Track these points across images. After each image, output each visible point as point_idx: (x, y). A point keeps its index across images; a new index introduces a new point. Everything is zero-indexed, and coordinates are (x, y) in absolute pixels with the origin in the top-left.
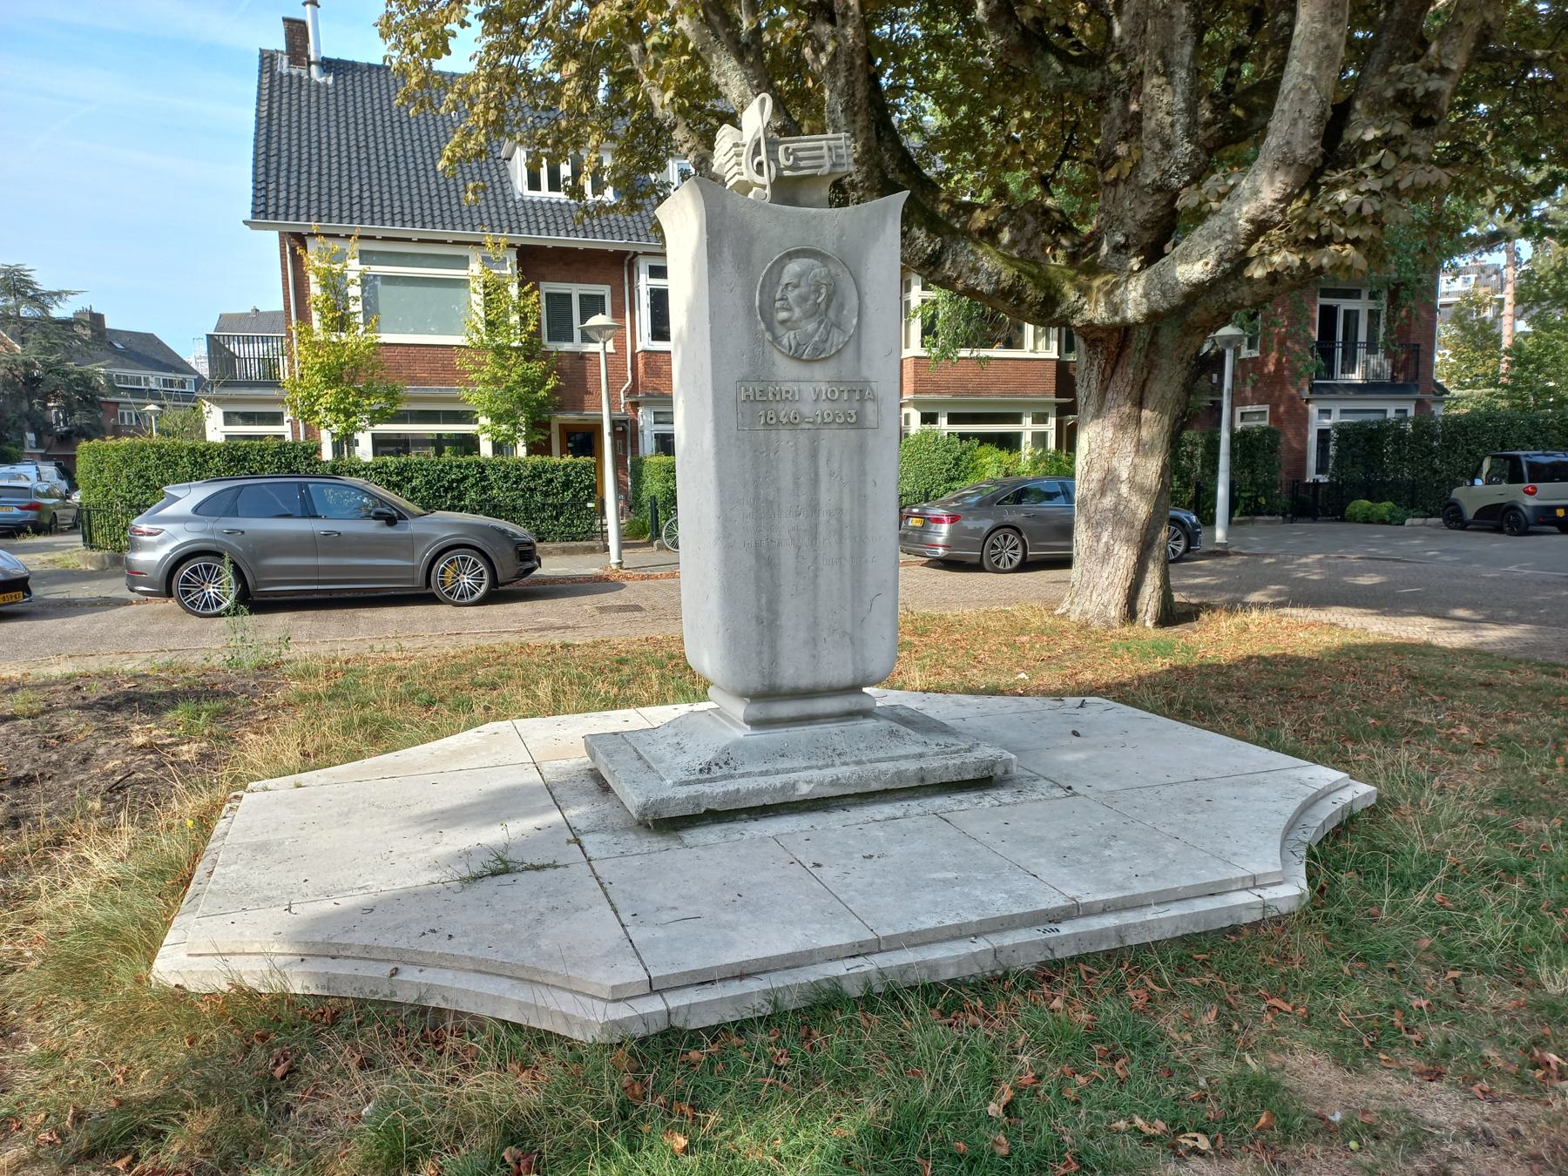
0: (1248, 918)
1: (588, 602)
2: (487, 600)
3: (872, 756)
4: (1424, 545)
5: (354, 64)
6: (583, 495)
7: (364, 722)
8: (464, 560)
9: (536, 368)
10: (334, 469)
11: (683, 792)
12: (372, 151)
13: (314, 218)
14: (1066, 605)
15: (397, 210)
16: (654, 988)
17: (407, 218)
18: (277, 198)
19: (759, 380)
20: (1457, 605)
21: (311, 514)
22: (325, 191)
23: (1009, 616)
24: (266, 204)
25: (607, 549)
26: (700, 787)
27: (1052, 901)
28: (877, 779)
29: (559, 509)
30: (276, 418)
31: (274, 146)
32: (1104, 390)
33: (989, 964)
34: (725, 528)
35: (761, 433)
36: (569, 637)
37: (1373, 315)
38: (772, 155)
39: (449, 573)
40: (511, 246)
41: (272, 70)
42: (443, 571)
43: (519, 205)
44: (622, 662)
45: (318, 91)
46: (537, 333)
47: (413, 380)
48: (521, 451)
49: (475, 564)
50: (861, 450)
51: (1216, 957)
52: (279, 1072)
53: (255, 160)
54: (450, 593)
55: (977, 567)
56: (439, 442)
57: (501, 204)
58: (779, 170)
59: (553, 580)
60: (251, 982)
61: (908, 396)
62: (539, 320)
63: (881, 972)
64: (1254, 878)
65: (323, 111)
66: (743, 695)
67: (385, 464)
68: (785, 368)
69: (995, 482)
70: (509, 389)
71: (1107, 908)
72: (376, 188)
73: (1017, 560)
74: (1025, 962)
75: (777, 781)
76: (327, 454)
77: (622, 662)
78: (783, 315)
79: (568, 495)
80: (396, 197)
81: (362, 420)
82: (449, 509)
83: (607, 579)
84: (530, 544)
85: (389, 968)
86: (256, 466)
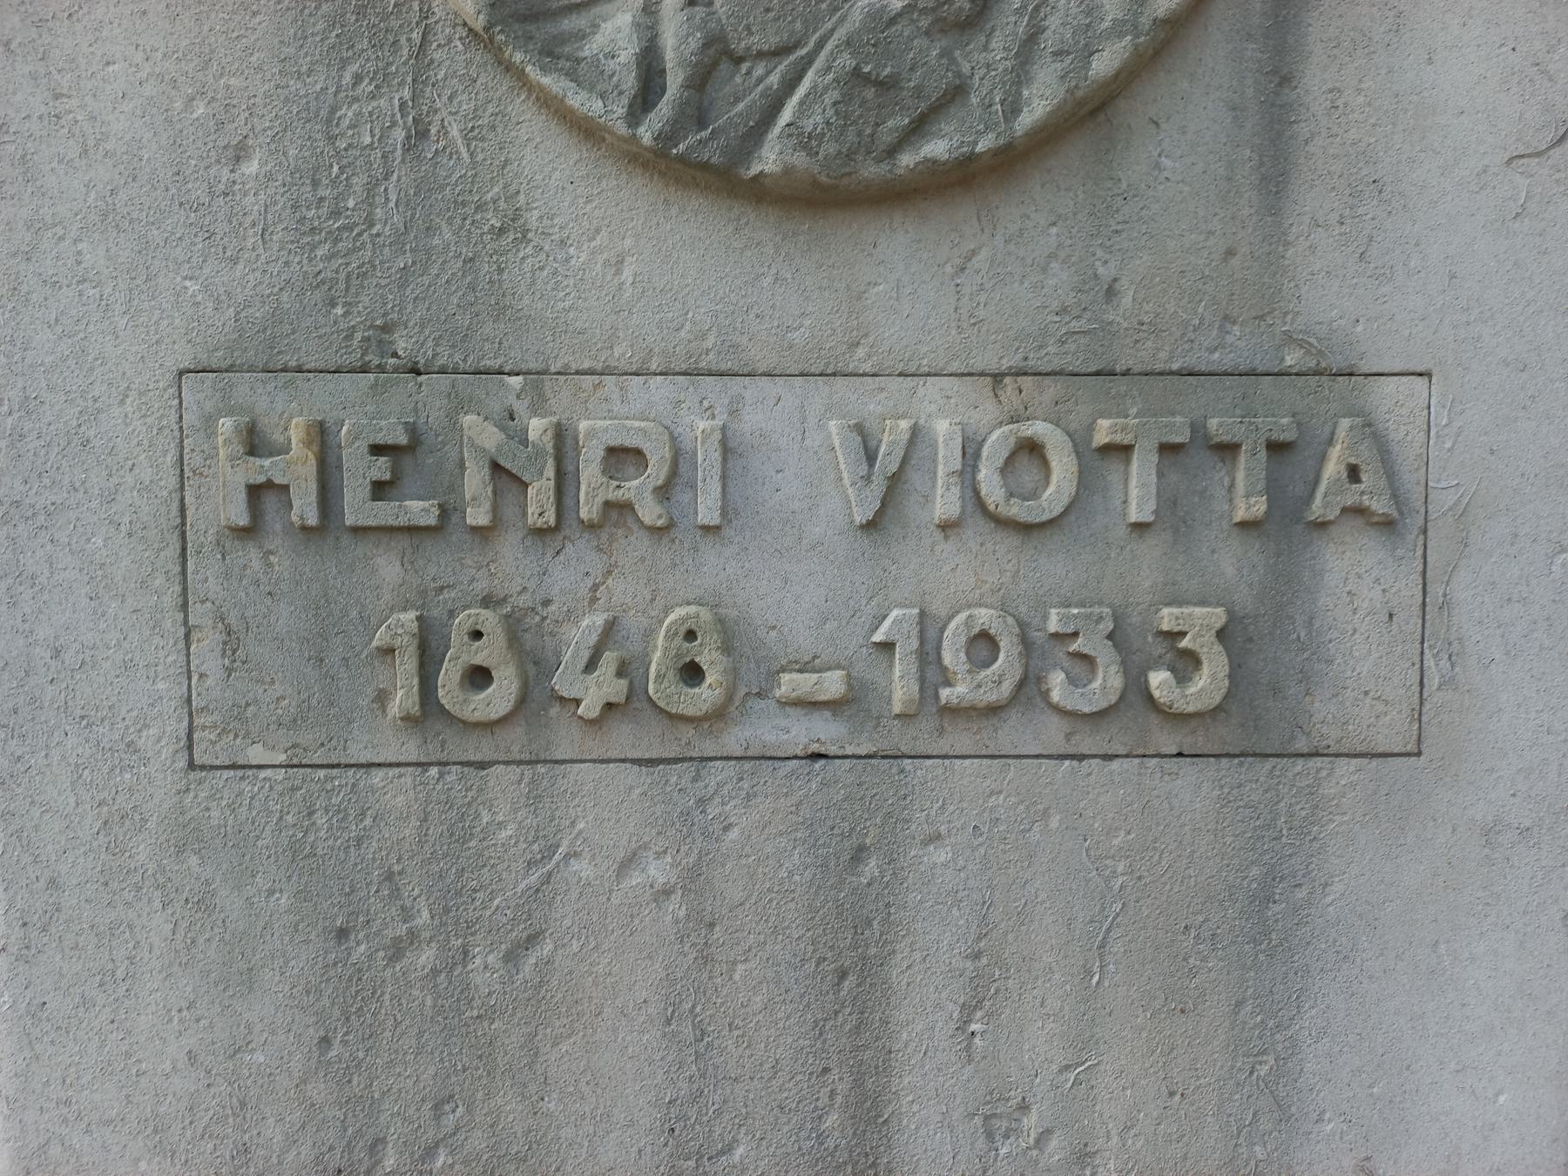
19: (376, 358)
35: (396, 794)
50: (1264, 928)
68: (617, 275)
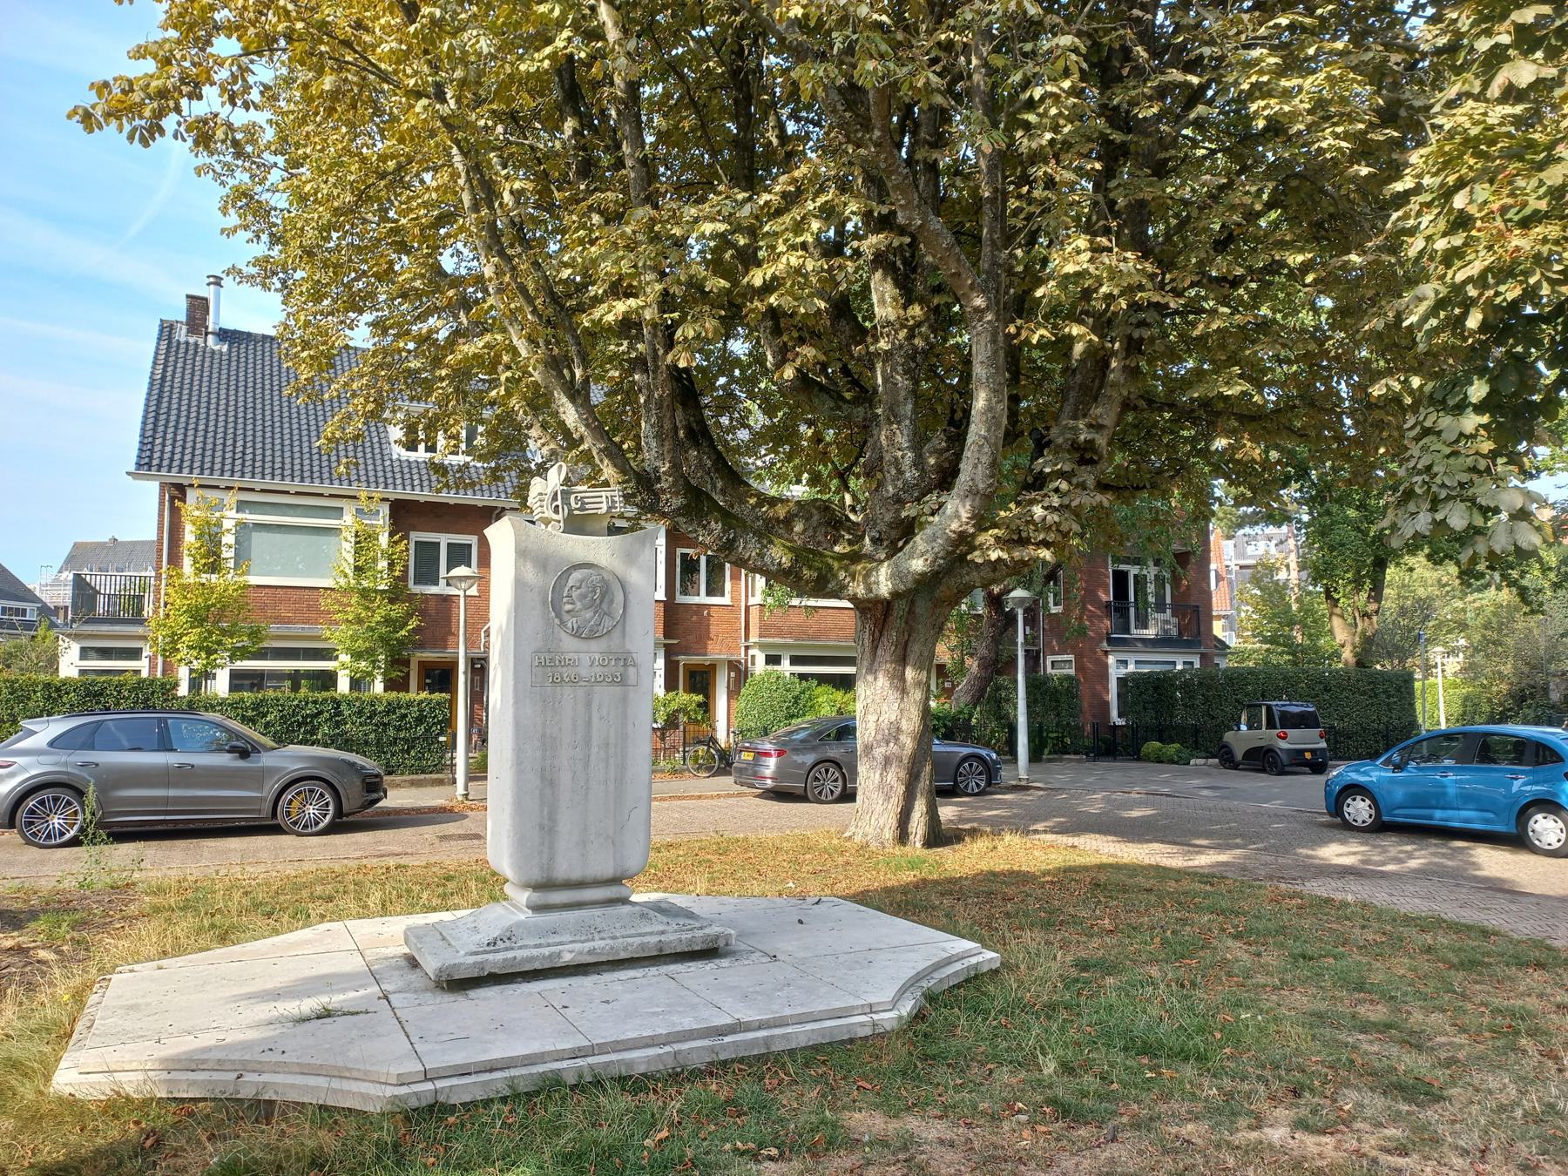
0: (862, 1032)
1: (429, 832)
2: (332, 829)
3: (625, 933)
4: (1199, 784)
5: (249, 334)
6: (436, 729)
7: (213, 926)
8: (311, 791)
9: (398, 610)
10: (190, 704)
11: (471, 960)
12: (259, 412)
13: (197, 471)
14: (852, 829)
15: (277, 465)
16: (427, 1077)
17: (287, 472)
18: (162, 452)
20: (1199, 836)
21: (165, 746)
22: (209, 446)
23: (804, 838)
24: (151, 457)
25: (454, 781)
26: (486, 956)
27: (724, 1020)
28: (625, 949)
29: (411, 744)
30: (135, 654)
31: (165, 405)
32: (875, 649)
33: (670, 1063)
34: (518, 757)
36: (403, 861)
37: (1160, 581)
38: (566, 501)
39: (295, 804)
40: (384, 500)
41: (170, 339)
42: (290, 802)
43: (396, 464)
44: (449, 878)
45: (212, 358)
46: (404, 577)
47: (279, 620)
48: (378, 687)
49: (322, 795)
50: (624, 700)
51: (836, 1059)
52: (149, 1143)
53: (145, 417)
54: (295, 823)
55: (802, 798)
56: (295, 678)
57: (379, 462)
58: (570, 510)
59: (398, 811)
60: (129, 1090)
61: (753, 639)
62: (406, 567)
63: (591, 1067)
64: (871, 1006)
65: (215, 375)
66: (527, 885)
67: (242, 700)
68: (569, 644)
69: (829, 720)
70: (372, 629)
71: (761, 1026)
72: (259, 445)
73: (838, 791)
74: (698, 1062)
75: (546, 951)
76: (183, 690)
77: (449, 878)
78: (568, 607)
79: (421, 730)
80: (278, 453)
81: (222, 657)
82: (300, 743)
83: (451, 811)
84: (377, 776)
85: (235, 1075)
86: (111, 701)
